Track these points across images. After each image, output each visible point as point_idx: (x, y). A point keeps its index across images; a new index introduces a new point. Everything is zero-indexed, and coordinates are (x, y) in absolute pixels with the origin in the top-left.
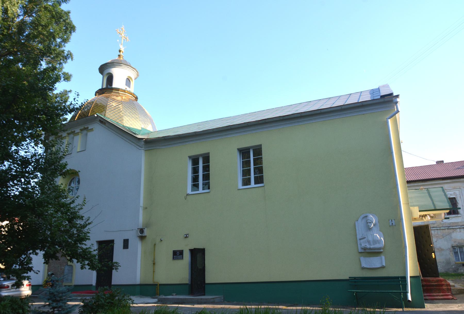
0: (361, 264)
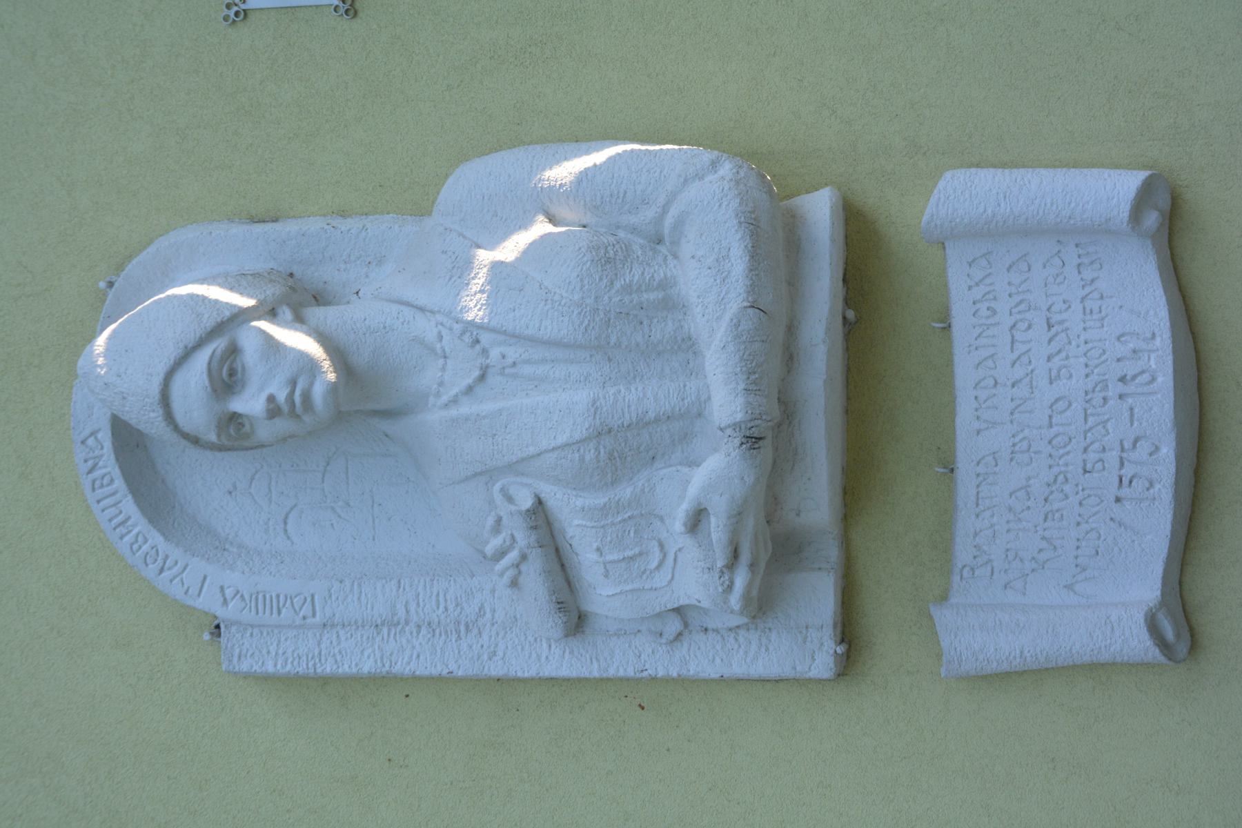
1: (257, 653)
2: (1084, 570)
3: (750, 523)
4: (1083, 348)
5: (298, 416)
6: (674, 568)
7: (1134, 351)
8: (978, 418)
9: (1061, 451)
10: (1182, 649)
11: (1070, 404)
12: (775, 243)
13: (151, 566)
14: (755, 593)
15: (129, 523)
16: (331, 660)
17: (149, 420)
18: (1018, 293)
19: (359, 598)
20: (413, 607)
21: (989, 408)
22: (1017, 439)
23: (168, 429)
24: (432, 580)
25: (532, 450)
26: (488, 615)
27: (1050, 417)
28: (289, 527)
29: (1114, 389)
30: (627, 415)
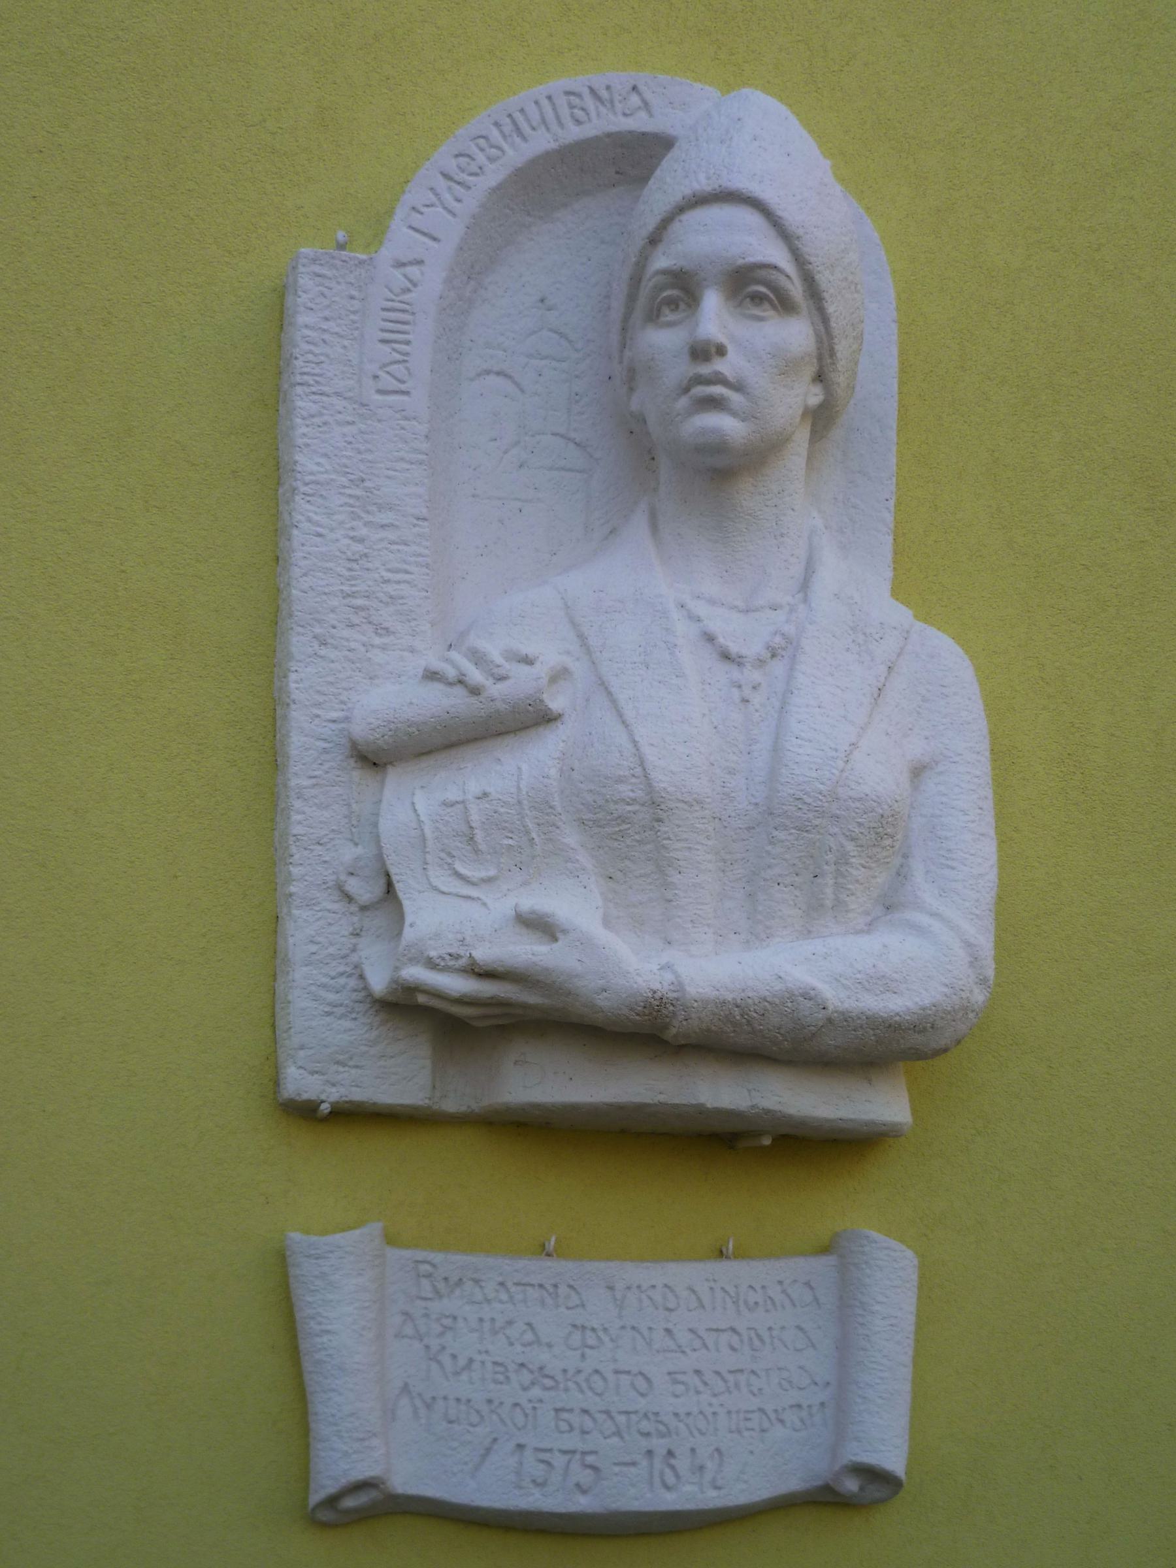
0: (277, 1083)
1: (326, 302)
3: (532, 998)
4: (708, 1411)
5: (686, 390)
6: (458, 896)
7: (701, 1468)
8: (629, 1288)
9: (584, 1385)
11: (642, 1395)
13: (454, 162)
14: (421, 999)
15: (518, 140)
16: (314, 408)
17: (673, 180)
18: (772, 1337)
19: (402, 459)
20: (391, 535)
21: (640, 1300)
22: (601, 1334)
23: (679, 197)
24: (427, 566)
25: (629, 714)
26: (377, 641)
27: (628, 1372)
29: (659, 1445)
30: (679, 845)
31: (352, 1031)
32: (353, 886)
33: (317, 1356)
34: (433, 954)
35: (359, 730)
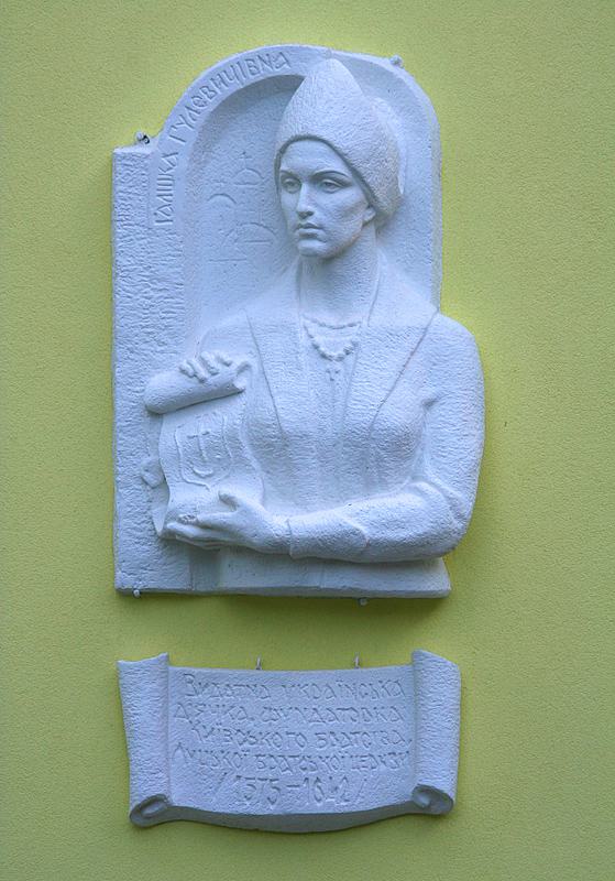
2: (192, 756)
10: (140, 821)
12: (412, 556)
26: (159, 349)
28: (219, 197)
31: (148, 551)
32: (147, 476)
33: (132, 728)
34: (181, 516)
35: (147, 400)
